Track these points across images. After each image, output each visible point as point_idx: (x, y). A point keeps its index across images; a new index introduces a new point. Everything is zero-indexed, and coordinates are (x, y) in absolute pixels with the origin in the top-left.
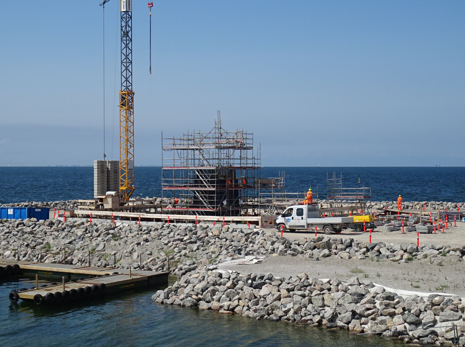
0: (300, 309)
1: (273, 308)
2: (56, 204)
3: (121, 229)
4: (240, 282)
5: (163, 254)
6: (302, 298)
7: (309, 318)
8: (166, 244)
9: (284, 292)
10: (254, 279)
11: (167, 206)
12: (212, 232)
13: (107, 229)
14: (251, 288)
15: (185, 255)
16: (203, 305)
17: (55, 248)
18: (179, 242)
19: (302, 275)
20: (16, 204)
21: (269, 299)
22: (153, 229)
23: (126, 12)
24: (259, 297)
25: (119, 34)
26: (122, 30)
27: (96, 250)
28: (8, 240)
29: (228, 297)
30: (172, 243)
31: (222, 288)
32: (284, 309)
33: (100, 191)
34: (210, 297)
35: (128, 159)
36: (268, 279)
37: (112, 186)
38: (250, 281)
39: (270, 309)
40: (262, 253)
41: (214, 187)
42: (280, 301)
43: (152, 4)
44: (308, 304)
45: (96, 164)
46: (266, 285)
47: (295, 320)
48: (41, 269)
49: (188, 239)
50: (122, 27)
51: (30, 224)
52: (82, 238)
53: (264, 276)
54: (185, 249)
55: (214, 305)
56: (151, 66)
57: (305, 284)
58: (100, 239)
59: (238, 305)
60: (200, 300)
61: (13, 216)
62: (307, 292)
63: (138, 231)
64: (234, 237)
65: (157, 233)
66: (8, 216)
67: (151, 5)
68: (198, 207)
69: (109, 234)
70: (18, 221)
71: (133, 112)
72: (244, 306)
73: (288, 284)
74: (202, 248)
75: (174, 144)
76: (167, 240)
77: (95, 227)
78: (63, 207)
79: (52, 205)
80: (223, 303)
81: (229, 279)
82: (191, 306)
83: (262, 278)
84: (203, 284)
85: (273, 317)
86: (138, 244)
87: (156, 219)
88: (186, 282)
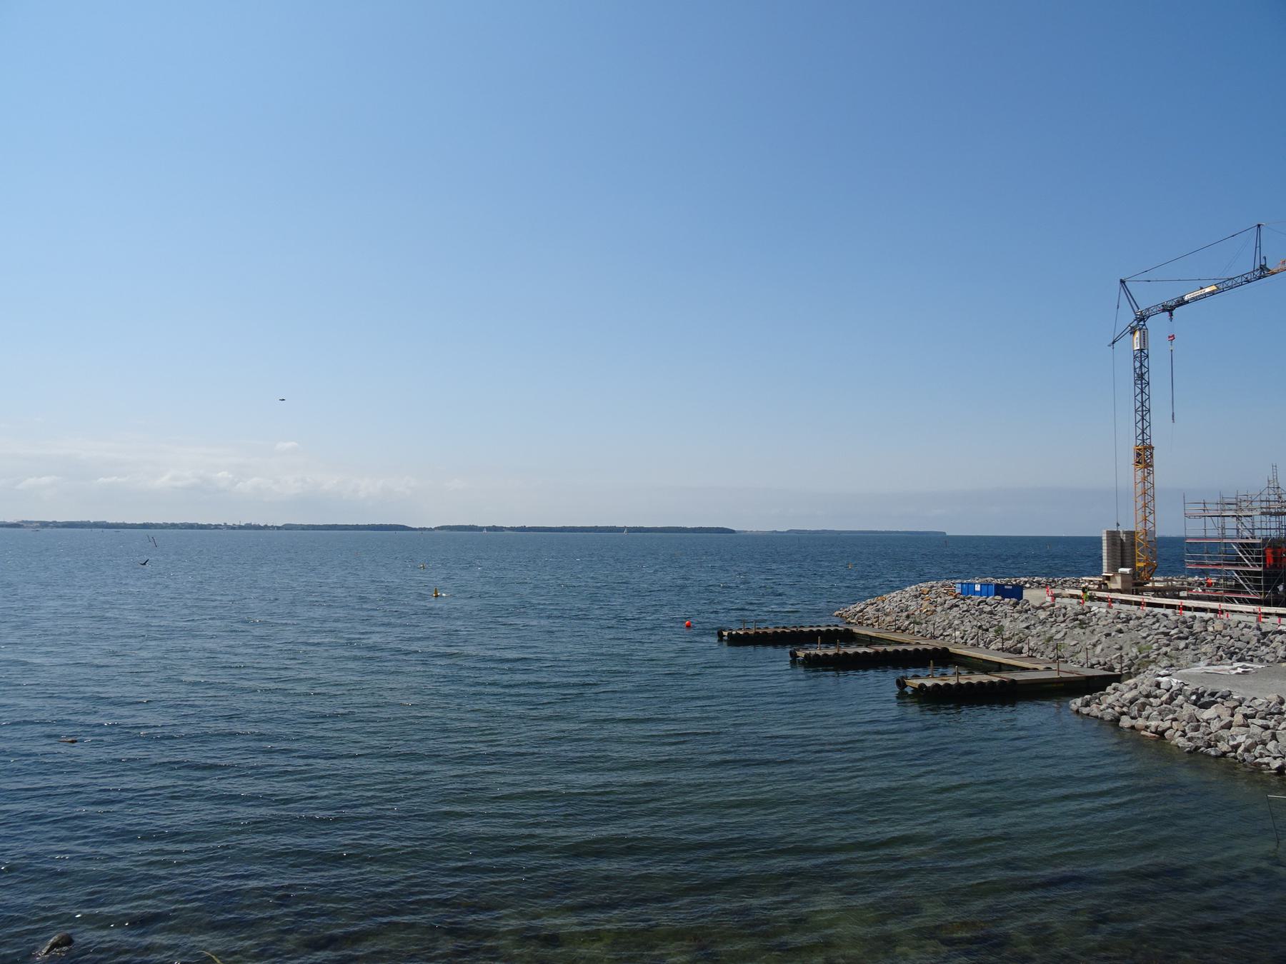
0: (1255, 745)
1: (1217, 738)
2: (1066, 581)
3: (1095, 615)
4: (1180, 697)
5: (1135, 650)
6: (1262, 730)
7: (1267, 762)
8: (1145, 638)
9: (1238, 718)
10: (1202, 695)
11: (1194, 589)
12: (1213, 627)
13: (1077, 614)
14: (1194, 707)
15: (1166, 654)
16: (1126, 722)
17: (1007, 633)
18: (1162, 636)
19: (1273, 698)
20: (1013, 579)
21: (1215, 725)
22: (1134, 617)
23: (1141, 350)
24: (1201, 720)
25: (1131, 377)
26: (1135, 372)
27: (1054, 638)
28: (963, 619)
29: (1160, 714)
30: (1151, 637)
31: (1157, 701)
32: (1232, 743)
33: (1110, 568)
34: (1136, 712)
35: (1147, 529)
36: (1222, 697)
37: (1128, 561)
38: (1194, 697)
39: (1213, 739)
40: (1268, 661)
41: (1260, 566)
42: (1230, 729)
43: (1173, 336)
44: (1271, 740)
45: (1105, 535)
46: (1215, 705)
47: (1244, 760)
48: (978, 657)
49: (1177, 634)
50: (1135, 369)
51: (993, 602)
52: (1043, 622)
53: (1217, 693)
54: (1168, 645)
55: (1138, 723)
56: (1173, 413)
57: (1272, 710)
58: (1063, 625)
59: (1171, 728)
60: (1123, 713)
61: (980, 593)
62: (1272, 723)
63: (1114, 619)
64: (1243, 635)
65: (1137, 622)
66: (975, 593)
67: (1172, 338)
68: (1239, 593)
69: (1077, 619)
70: (983, 598)
71: (1153, 471)
72: (1177, 730)
73: (1248, 707)
74: (1192, 647)
75: (1204, 510)
76: (1147, 633)
77: (1063, 611)
78: (1075, 585)
79: (1060, 583)
80: (1150, 723)
81: (1168, 691)
82: (1112, 720)
83: (1213, 694)
84: (1134, 693)
85: (1212, 752)
86: (1108, 635)
87: (1166, 605)
88: (1114, 689)
